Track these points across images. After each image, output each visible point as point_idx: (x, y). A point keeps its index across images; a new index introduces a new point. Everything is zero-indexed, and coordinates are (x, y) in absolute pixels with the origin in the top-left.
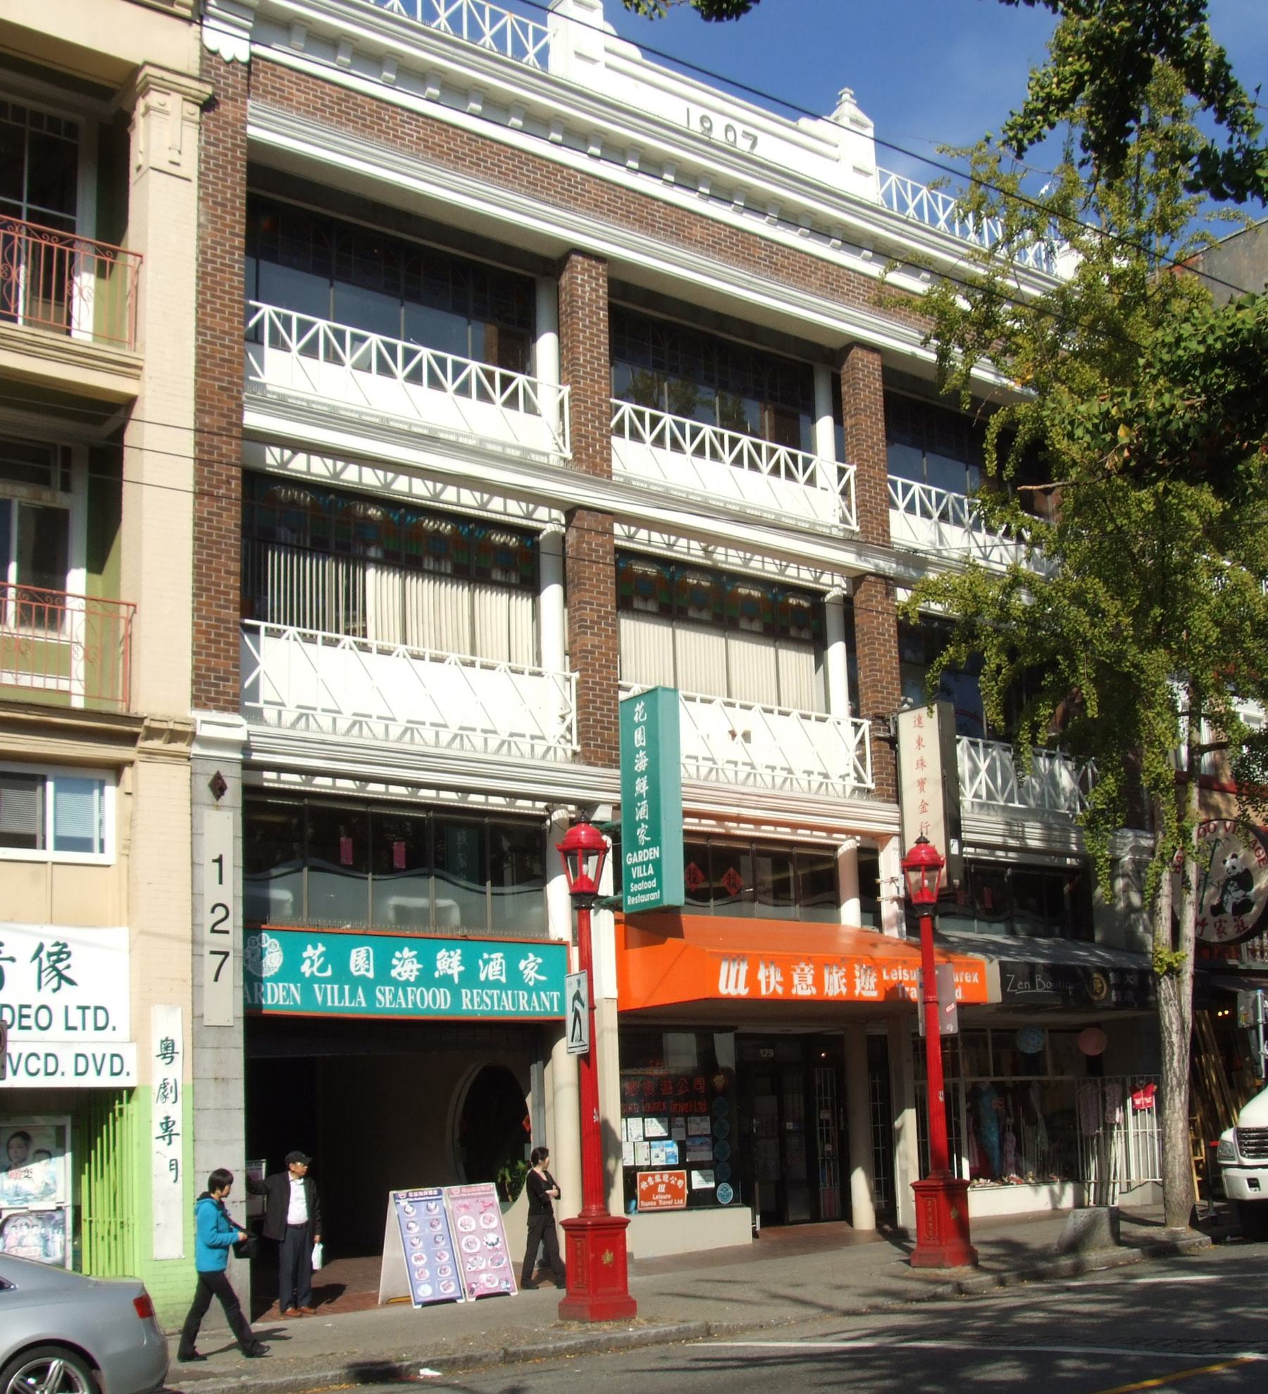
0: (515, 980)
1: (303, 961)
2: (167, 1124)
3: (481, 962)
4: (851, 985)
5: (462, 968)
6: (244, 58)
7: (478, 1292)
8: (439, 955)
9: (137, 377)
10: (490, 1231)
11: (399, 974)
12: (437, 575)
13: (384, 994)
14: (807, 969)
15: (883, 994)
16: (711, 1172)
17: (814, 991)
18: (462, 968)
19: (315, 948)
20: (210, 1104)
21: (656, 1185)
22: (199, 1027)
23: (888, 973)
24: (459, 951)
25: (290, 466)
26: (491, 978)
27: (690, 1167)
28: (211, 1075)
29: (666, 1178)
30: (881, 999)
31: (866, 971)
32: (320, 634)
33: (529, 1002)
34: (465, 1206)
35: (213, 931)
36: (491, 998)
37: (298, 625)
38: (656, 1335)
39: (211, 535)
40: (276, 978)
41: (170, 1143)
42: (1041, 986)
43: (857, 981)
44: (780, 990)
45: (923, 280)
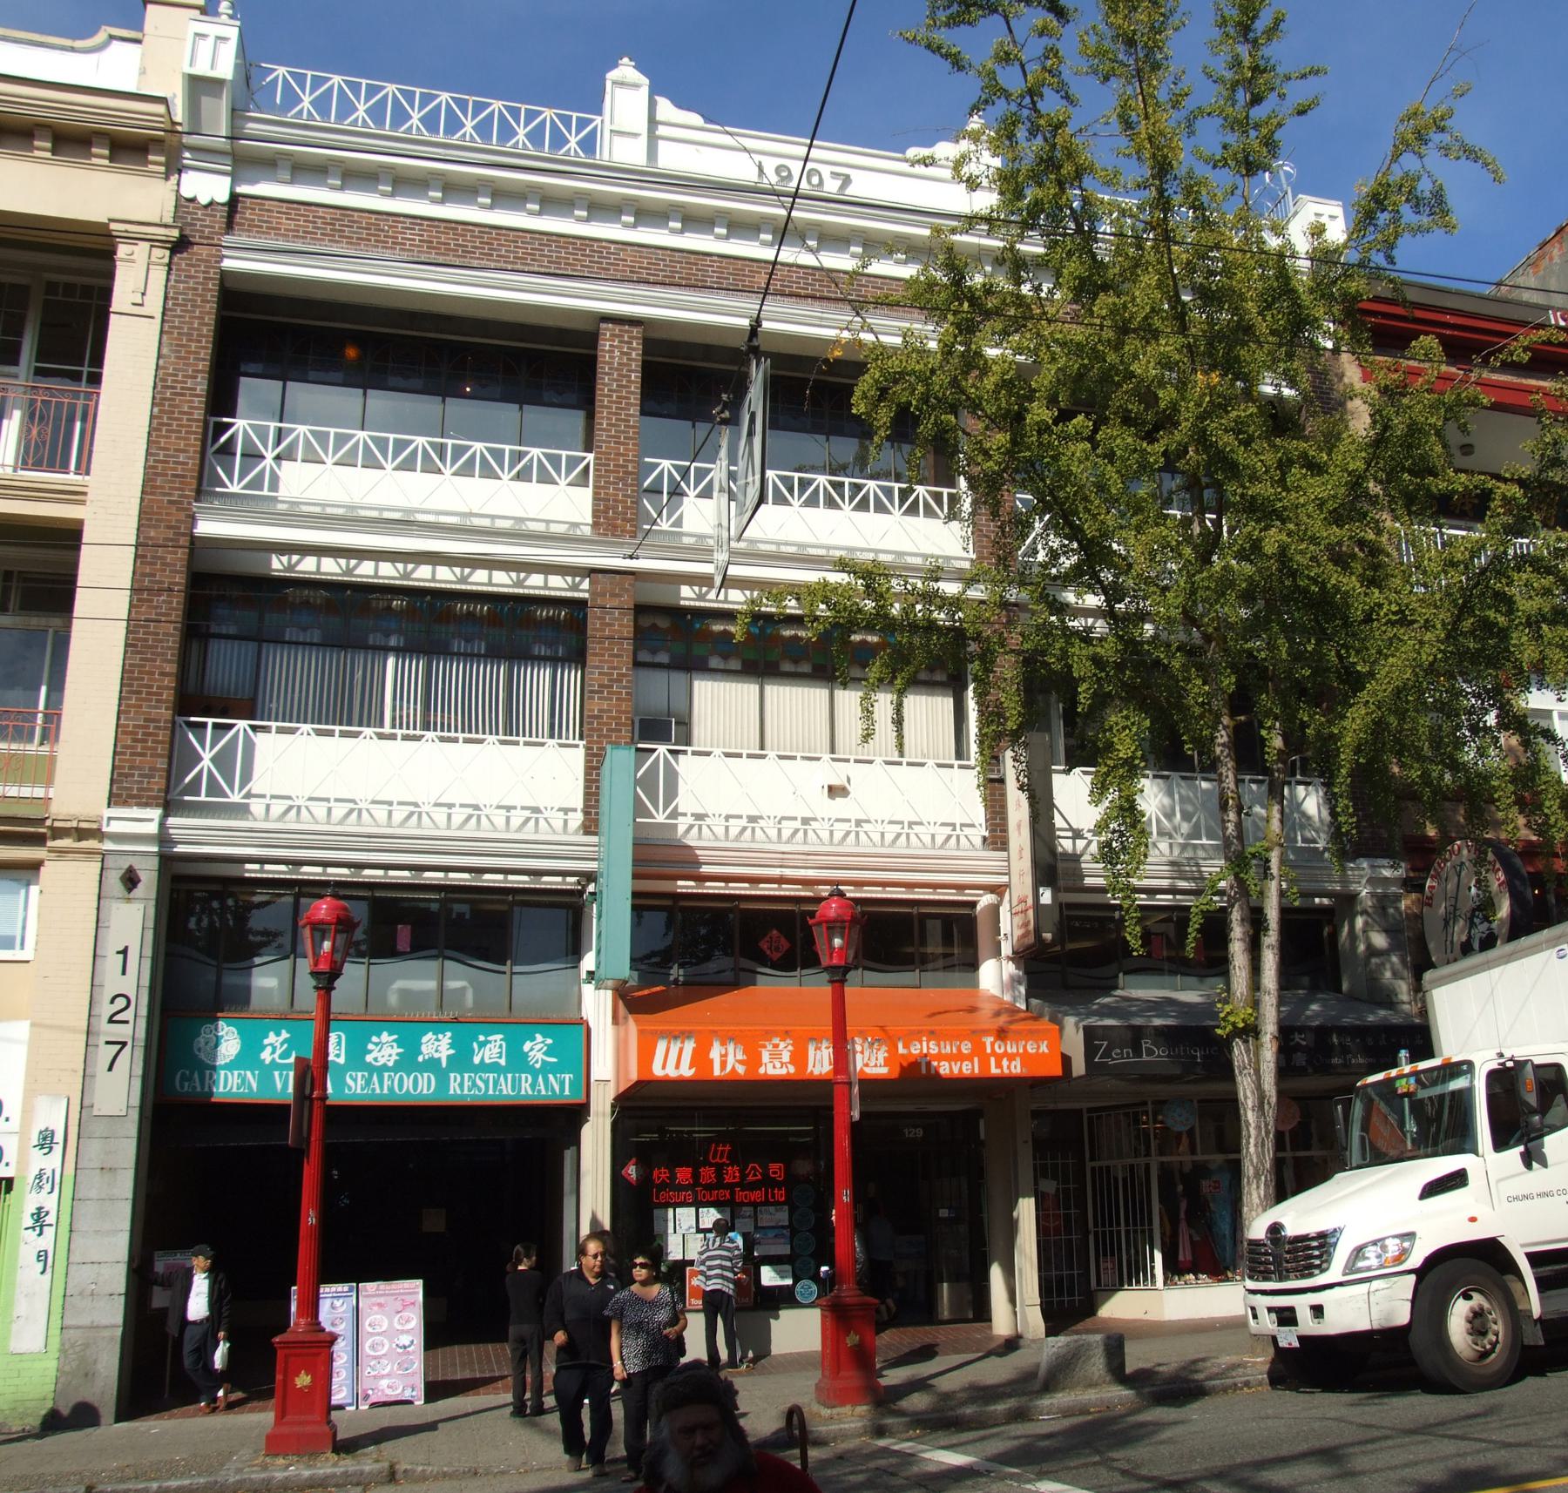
0: (518, 1062)
1: (263, 1047)
2: (39, 1215)
3: (475, 1045)
5: (452, 1052)
6: (223, 197)
7: (374, 1399)
8: (424, 1039)
9: (83, 503)
10: (403, 1332)
11: (376, 1059)
12: (727, 674)
13: (355, 1080)
14: (782, 1045)
15: (898, 1070)
16: (788, 1268)
17: (792, 1069)
18: (452, 1052)
19: (278, 1034)
20: (93, 1194)
22: (85, 1116)
23: (905, 1047)
24: (449, 1034)
25: (357, 572)
26: (487, 1061)
28: (98, 1165)
30: (895, 1075)
31: (871, 1045)
32: (337, 728)
33: (533, 1086)
34: (380, 1305)
35: (111, 1021)
36: (486, 1082)
37: (560, 737)
38: (311, 1478)
39: (146, 640)
40: (230, 1066)
41: (41, 1234)
42: (1150, 1052)
44: (741, 1070)
45: (854, 256)
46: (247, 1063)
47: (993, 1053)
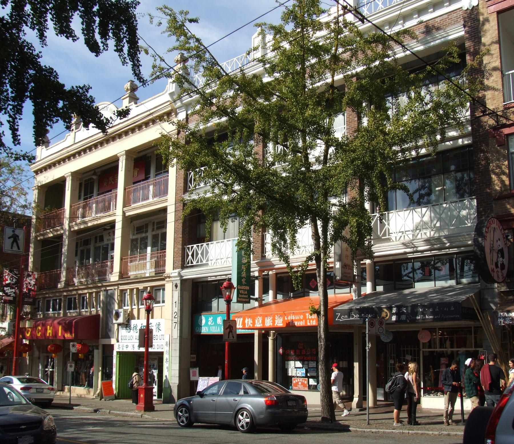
4: (274, 322)
17: (262, 325)
21: (298, 382)
22: (171, 336)
27: (309, 378)
29: (301, 380)
43: (276, 321)
46: (211, 325)
47: (308, 318)
